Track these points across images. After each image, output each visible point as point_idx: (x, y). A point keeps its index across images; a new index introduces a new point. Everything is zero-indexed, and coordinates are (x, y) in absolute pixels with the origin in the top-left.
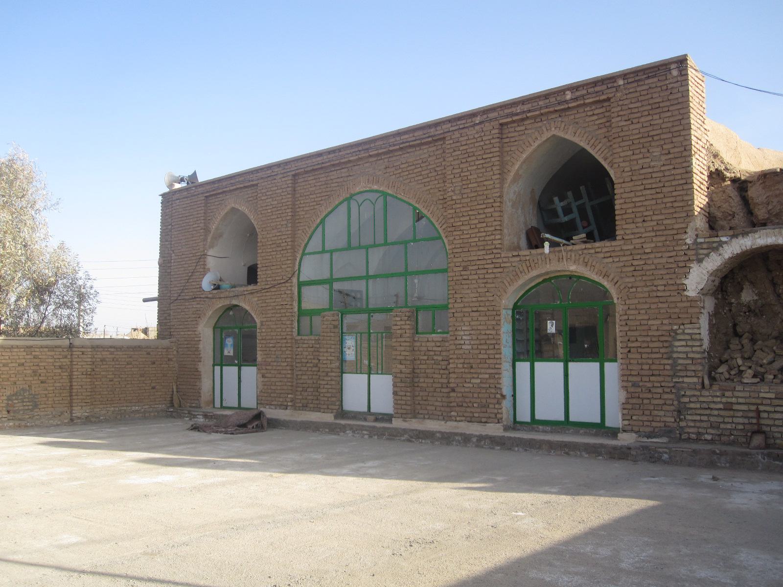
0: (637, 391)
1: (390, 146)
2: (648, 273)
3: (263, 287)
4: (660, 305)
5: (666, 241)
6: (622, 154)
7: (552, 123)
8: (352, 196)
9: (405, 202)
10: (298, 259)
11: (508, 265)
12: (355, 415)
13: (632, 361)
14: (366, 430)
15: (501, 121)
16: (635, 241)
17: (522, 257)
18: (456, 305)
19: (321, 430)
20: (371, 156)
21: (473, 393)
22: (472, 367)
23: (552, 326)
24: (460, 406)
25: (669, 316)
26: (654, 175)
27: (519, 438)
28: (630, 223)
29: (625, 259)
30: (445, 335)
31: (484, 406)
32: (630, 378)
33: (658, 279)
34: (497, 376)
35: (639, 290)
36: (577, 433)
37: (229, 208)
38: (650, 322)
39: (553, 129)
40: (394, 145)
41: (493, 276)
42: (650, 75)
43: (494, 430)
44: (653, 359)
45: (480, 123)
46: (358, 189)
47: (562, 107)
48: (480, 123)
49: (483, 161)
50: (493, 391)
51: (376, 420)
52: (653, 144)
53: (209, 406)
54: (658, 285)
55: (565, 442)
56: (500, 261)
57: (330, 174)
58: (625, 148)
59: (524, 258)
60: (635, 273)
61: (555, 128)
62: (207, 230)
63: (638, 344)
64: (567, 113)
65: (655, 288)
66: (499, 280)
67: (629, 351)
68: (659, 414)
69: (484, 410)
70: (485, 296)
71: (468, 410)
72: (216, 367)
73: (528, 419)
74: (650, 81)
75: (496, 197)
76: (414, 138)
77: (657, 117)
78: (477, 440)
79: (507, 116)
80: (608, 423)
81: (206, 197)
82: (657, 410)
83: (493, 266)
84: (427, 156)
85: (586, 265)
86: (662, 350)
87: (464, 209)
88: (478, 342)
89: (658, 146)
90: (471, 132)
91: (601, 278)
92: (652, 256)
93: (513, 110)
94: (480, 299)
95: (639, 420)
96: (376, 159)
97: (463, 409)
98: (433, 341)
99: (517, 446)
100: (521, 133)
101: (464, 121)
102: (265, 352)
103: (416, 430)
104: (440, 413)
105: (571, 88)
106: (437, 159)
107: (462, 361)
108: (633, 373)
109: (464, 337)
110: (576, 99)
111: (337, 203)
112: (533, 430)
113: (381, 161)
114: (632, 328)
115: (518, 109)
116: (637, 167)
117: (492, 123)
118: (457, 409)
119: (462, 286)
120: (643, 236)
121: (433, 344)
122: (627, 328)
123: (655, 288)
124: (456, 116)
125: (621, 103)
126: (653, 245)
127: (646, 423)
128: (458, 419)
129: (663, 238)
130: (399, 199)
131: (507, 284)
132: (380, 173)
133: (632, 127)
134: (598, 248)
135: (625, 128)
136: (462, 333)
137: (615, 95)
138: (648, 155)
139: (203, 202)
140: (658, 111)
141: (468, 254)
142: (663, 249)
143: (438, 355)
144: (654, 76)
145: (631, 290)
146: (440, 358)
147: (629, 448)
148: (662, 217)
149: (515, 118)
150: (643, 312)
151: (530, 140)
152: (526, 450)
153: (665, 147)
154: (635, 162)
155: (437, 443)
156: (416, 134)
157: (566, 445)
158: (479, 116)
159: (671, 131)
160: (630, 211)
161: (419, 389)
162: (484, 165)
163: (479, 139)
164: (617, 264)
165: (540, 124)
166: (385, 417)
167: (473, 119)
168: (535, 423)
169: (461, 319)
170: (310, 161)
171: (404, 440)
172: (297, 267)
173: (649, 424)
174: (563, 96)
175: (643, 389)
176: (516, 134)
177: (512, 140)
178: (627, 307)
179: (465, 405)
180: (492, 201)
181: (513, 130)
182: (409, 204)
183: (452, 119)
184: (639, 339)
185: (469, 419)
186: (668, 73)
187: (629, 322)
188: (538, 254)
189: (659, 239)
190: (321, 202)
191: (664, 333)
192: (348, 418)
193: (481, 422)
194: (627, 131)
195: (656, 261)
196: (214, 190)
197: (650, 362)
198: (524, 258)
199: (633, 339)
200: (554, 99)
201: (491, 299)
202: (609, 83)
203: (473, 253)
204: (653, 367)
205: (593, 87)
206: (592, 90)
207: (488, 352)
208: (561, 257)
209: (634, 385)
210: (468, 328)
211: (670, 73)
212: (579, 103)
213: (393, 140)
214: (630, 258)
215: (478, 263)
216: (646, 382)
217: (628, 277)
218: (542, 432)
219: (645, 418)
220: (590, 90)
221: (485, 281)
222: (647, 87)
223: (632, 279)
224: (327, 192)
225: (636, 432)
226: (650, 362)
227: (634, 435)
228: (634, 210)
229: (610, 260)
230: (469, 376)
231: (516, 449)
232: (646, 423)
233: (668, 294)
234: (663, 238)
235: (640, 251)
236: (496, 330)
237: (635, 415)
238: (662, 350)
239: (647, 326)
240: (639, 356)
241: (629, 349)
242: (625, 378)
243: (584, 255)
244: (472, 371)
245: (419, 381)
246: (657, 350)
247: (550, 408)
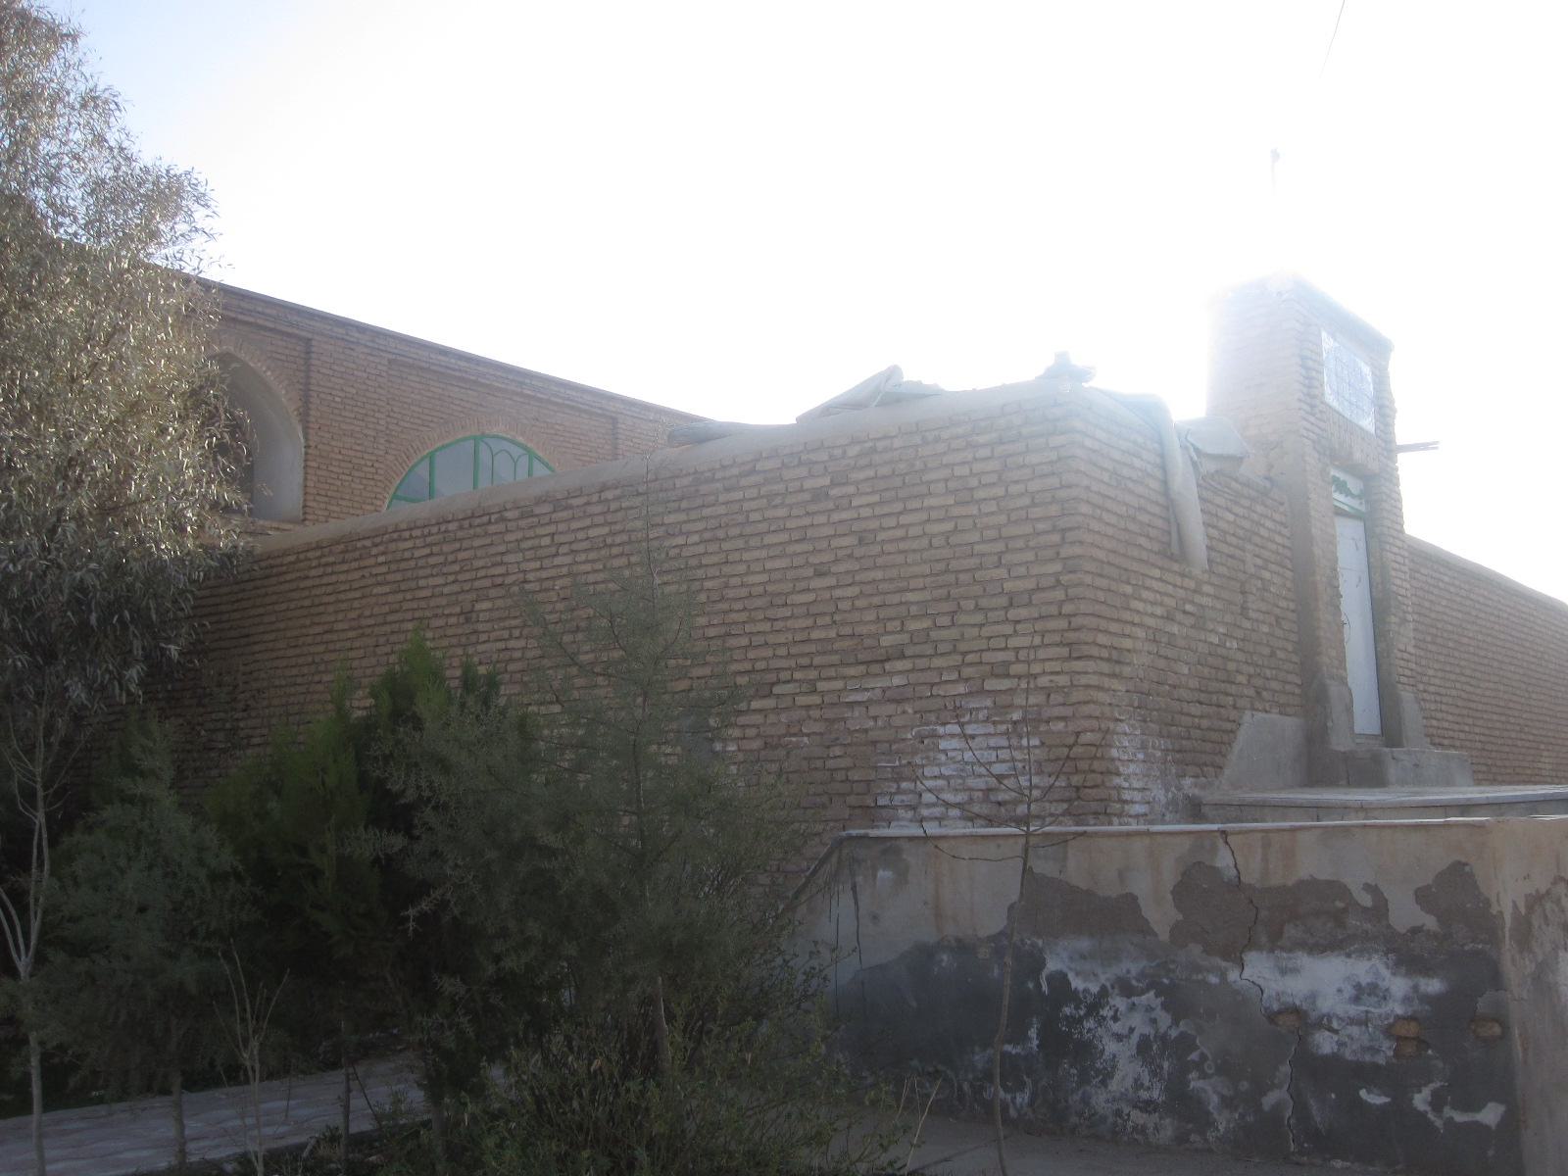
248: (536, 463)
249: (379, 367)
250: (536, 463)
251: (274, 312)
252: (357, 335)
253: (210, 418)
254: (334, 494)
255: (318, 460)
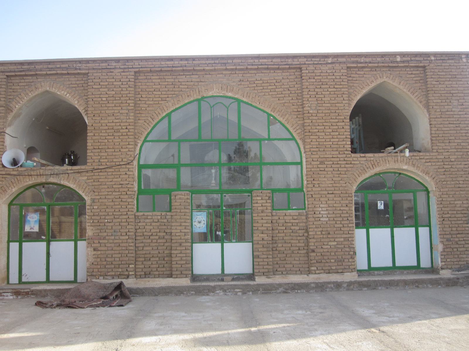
0: (450, 244)
1: (248, 65)
2: (453, 173)
3: (95, 167)
4: (461, 192)
5: (463, 155)
6: (435, 101)
7: (384, 74)
8: (203, 98)
9: (259, 109)
10: (139, 145)
11: (358, 162)
12: (208, 278)
13: (446, 226)
14: (239, 289)
15: (348, 65)
16: (444, 154)
17: (367, 158)
18: (314, 189)
19: (185, 293)
20: (226, 69)
21: (331, 252)
22: (329, 234)
23: (381, 204)
24: (319, 262)
25: (466, 199)
26: (455, 116)
27: (381, 280)
28: (441, 143)
29: (439, 164)
30: (301, 211)
31: (341, 261)
32: (445, 236)
33: (459, 177)
34: (350, 239)
35: (448, 183)
36: (402, 273)
37: (40, 90)
38: (456, 202)
39: (385, 78)
40: (252, 65)
41: (345, 169)
42: (450, 58)
43: (350, 277)
44: (458, 224)
45: (332, 63)
46: (210, 94)
47: (394, 65)
48: (331, 63)
49: (335, 90)
50: (348, 249)
51: (233, 280)
52: (453, 98)
53: (4, 283)
54: (460, 181)
55: (415, 279)
56: (351, 159)
57: (178, 77)
58: (436, 98)
59: (369, 159)
60: (446, 173)
61: (386, 77)
62: (9, 110)
63: (449, 216)
64: (394, 69)
65: (458, 182)
66: (351, 173)
67: (443, 220)
68: (463, 257)
69: (340, 263)
70: (339, 183)
71: (327, 264)
72: (11, 244)
73: (366, 267)
74: (450, 61)
75: (346, 115)
76: (273, 63)
77: (454, 83)
78: (348, 285)
79: (353, 62)
80: (422, 265)
81: (7, 76)
82: (462, 254)
83: (345, 162)
84: (281, 78)
85: (414, 166)
86: (464, 219)
87: (320, 121)
88: (334, 216)
89: (456, 100)
90: (324, 68)
91: (424, 174)
92: (455, 163)
93: (358, 59)
94: (334, 185)
95: (451, 261)
96: (230, 72)
97: (322, 265)
98: (290, 215)
99: (380, 286)
100: (361, 76)
101: (318, 59)
102: (99, 227)
103: (292, 283)
104: (298, 269)
105: (401, 54)
106: (290, 82)
107: (321, 229)
108: (447, 233)
109: (322, 212)
110: (403, 62)
111: (186, 102)
112: (370, 274)
113: (236, 75)
114: (445, 206)
115: (362, 60)
116: (444, 110)
117: (341, 65)
118: (317, 265)
119: (319, 175)
120: (450, 151)
121: (291, 218)
122: (442, 206)
123: (458, 182)
124: (312, 55)
125: (433, 70)
126: (456, 157)
127: (455, 263)
128: (317, 272)
129: (461, 153)
130: (253, 106)
131: (357, 176)
132: (234, 84)
133: (440, 86)
134: (422, 156)
135: (436, 86)
136: (320, 209)
137: (429, 65)
138: (451, 104)
139: (5, 80)
140: (455, 79)
141: (324, 153)
142: (462, 160)
143: (295, 226)
144: (452, 59)
145: (444, 183)
146: (297, 228)
147: (458, 279)
148: (460, 141)
149: (359, 65)
150: (451, 196)
151: (368, 81)
152: (387, 288)
153: (460, 101)
154: (443, 107)
155: (312, 291)
156: (274, 60)
157: (417, 281)
158: (331, 58)
159: (463, 92)
160: (441, 135)
161: (277, 252)
162: (336, 92)
163: (331, 74)
164: (434, 166)
165: (375, 73)
166: (241, 276)
167: (326, 60)
168: (371, 270)
169: (318, 199)
170: (159, 63)
171: (280, 293)
172: (137, 152)
173: (457, 263)
174: (395, 58)
175: (453, 242)
176: (357, 76)
177: (355, 79)
178: (441, 193)
179: (323, 261)
180: (343, 117)
181: (354, 72)
182: (264, 112)
183: (307, 56)
184: (450, 212)
185: (327, 271)
186: (460, 59)
187: (443, 203)
188: (379, 157)
189: (459, 153)
190: (167, 99)
191: (464, 209)
192: (200, 281)
193: (338, 273)
194: (437, 88)
195: (458, 166)
196: (21, 71)
197: (457, 226)
198: (369, 159)
199: (446, 212)
200: (388, 59)
201: (344, 185)
202: (425, 57)
203: (327, 153)
204: (459, 229)
205: (414, 57)
206: (414, 58)
207: (342, 222)
208: (396, 160)
209: (448, 240)
210: (326, 206)
211: (461, 60)
212: (405, 64)
213: (252, 61)
214: (442, 163)
215: (333, 159)
216: (454, 238)
217: (442, 175)
218: (376, 275)
219: (455, 260)
220: (413, 59)
221: (339, 172)
222: (448, 65)
223: (444, 176)
224: (175, 91)
225: (450, 269)
226: (457, 226)
227: (449, 270)
228: (443, 135)
229: (430, 164)
230: (327, 240)
231: (380, 288)
232: (455, 263)
233: (465, 186)
234: (461, 153)
235: (448, 160)
236: (349, 207)
237: (448, 258)
238: (464, 219)
239: (454, 205)
240: (450, 223)
241: (443, 219)
242: (442, 236)
243: (412, 160)
244: (329, 236)
245: (277, 246)
246: (460, 219)
247: (381, 258)
248: (148, 139)
249: (129, 77)
250: (148, 139)
251: (67, 66)
252: (115, 64)
253: (60, 225)
254: (104, 147)
255: (93, 131)
